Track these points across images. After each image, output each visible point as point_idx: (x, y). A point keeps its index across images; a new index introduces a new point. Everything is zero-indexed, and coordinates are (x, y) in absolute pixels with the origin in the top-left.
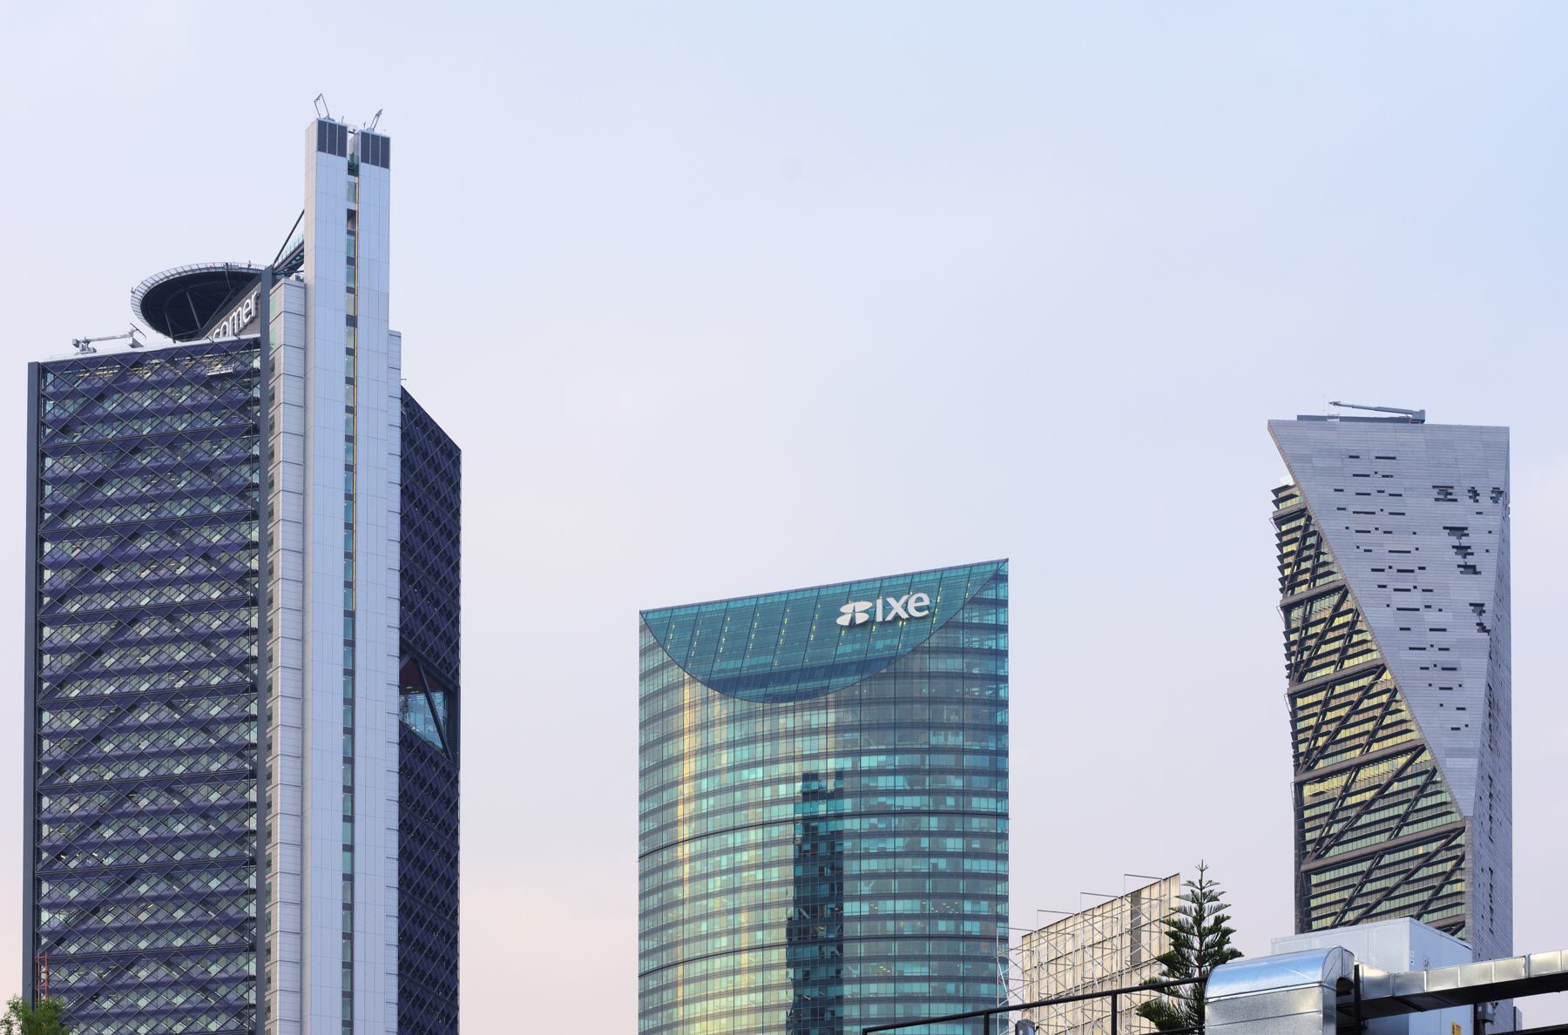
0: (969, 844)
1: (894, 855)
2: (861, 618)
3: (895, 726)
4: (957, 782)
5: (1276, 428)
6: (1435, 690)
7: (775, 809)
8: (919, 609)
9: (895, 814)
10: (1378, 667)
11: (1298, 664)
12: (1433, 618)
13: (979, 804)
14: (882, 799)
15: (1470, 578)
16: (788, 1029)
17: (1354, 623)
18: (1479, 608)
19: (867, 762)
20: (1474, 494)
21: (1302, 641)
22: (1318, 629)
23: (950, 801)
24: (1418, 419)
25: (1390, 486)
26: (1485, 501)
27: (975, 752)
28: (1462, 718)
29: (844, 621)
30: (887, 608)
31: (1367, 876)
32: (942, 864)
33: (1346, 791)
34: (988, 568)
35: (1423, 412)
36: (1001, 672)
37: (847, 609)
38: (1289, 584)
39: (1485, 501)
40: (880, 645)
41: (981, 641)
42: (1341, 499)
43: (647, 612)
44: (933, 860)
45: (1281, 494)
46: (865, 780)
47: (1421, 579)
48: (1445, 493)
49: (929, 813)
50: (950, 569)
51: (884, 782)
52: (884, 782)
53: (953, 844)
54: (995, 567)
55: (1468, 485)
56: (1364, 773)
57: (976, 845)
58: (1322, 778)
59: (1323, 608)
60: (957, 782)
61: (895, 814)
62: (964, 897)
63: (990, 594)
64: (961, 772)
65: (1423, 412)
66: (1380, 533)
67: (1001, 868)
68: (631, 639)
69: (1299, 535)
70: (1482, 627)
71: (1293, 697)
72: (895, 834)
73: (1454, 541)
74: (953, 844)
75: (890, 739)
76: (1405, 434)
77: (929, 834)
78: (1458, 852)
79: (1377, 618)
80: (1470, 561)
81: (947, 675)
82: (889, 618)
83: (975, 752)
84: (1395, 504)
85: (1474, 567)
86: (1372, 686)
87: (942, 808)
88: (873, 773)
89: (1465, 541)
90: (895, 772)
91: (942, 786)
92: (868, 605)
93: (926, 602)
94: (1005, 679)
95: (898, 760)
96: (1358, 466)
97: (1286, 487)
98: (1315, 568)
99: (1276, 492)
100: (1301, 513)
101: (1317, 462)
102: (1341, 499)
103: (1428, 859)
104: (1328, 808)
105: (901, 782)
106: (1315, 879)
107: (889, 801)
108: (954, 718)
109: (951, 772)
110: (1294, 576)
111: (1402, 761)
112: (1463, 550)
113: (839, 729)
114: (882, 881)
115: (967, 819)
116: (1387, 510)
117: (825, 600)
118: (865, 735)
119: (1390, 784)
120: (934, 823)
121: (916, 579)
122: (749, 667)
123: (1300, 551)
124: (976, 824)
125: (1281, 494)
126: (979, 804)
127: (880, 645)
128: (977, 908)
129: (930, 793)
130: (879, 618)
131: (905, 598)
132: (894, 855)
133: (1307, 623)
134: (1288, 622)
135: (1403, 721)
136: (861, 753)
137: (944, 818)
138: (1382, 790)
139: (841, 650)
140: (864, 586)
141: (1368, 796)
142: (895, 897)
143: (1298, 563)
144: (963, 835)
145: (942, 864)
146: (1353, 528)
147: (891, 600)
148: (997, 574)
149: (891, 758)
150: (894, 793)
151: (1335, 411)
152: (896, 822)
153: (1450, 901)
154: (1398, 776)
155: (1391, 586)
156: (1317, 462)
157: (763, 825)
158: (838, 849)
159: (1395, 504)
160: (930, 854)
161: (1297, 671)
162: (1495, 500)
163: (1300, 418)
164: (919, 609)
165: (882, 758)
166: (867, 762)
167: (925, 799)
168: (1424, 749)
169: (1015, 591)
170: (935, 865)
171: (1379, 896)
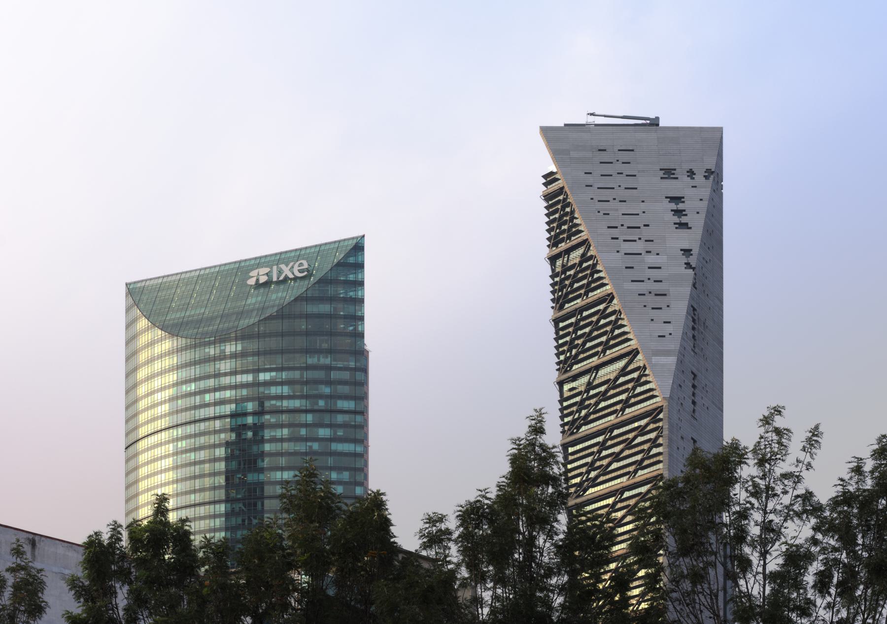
0: (335, 433)
1: (282, 440)
2: (263, 279)
3: (282, 352)
4: (327, 390)
5: (547, 132)
6: (648, 309)
7: (202, 410)
8: (300, 271)
9: (282, 412)
10: (608, 295)
11: (559, 298)
12: (651, 260)
13: (343, 404)
14: (273, 402)
15: (683, 232)
16: (87, 548)
17: (594, 265)
18: (687, 252)
19: (263, 377)
20: (691, 173)
21: (562, 281)
22: (572, 272)
23: (321, 403)
24: (655, 123)
25: (626, 169)
26: (699, 178)
27: (340, 369)
28: (669, 328)
29: (252, 282)
30: (280, 272)
31: (603, 446)
32: (316, 446)
33: (590, 386)
34: (350, 242)
35: (657, 118)
36: (359, 314)
37: (254, 273)
38: (554, 241)
39: (699, 178)
40: (274, 296)
41: (346, 293)
42: (590, 179)
43: (130, 284)
44: (309, 444)
45: (549, 179)
46: (261, 389)
47: (646, 233)
48: (669, 173)
49: (306, 411)
50: (326, 244)
51: (274, 390)
52: (274, 390)
53: (323, 432)
54: (355, 241)
55: (687, 167)
56: (602, 372)
57: (340, 433)
58: (575, 378)
59: (575, 256)
60: (327, 390)
61: (282, 412)
62: (331, 469)
63: (352, 260)
64: (329, 383)
65: (657, 118)
66: (616, 203)
67: (359, 449)
68: (120, 300)
69: (557, 203)
70: (688, 265)
71: (556, 321)
72: (282, 426)
73: (673, 206)
74: (323, 432)
75: (279, 360)
76: (651, 135)
77: (306, 425)
78: (660, 424)
79: (607, 261)
80: (684, 220)
81: (320, 316)
82: (281, 278)
83: (340, 369)
84: (631, 182)
85: (687, 224)
86: (606, 309)
87: (316, 407)
88: (267, 384)
89: (681, 206)
90: (282, 383)
91: (315, 392)
92: (267, 270)
93: (306, 266)
94: (362, 318)
95: (284, 375)
96: (605, 157)
97: (552, 173)
98: (570, 228)
99: (545, 177)
100: (561, 190)
101: (573, 154)
102: (590, 179)
103: (642, 431)
104: (578, 399)
105: (286, 390)
106: (571, 450)
107: (279, 403)
108: (325, 346)
109: (321, 382)
110: (557, 235)
111: (621, 364)
112: (678, 212)
113: (244, 354)
114: (273, 458)
115: (333, 415)
116: (623, 186)
117: (242, 268)
118: (262, 358)
119: (617, 379)
120: (310, 418)
121: (303, 252)
122: (189, 316)
123: (561, 217)
124: (340, 418)
125: (549, 179)
126: (343, 404)
127: (274, 296)
128: (341, 476)
129: (307, 397)
130: (275, 279)
131: (291, 264)
132: (282, 440)
133: (565, 268)
134: (553, 270)
135: (625, 333)
136: (259, 371)
137: (317, 415)
138: (612, 383)
139: (249, 301)
140: (268, 259)
141: (603, 389)
142: (282, 469)
143: (559, 227)
144: (330, 426)
145: (316, 446)
146: (596, 199)
147: (283, 266)
148: (358, 247)
149: (279, 374)
150: (281, 397)
151: (592, 119)
152: (284, 418)
153: (655, 459)
154: (623, 372)
155: (622, 238)
156: (573, 154)
157: (195, 422)
158: (243, 437)
159: (631, 182)
160: (306, 439)
161: (559, 302)
162: (706, 177)
163: (566, 125)
164: (300, 271)
165: (273, 374)
166: (263, 377)
167: (304, 401)
168: (638, 353)
169: (369, 258)
170: (311, 447)
171: (609, 459)
